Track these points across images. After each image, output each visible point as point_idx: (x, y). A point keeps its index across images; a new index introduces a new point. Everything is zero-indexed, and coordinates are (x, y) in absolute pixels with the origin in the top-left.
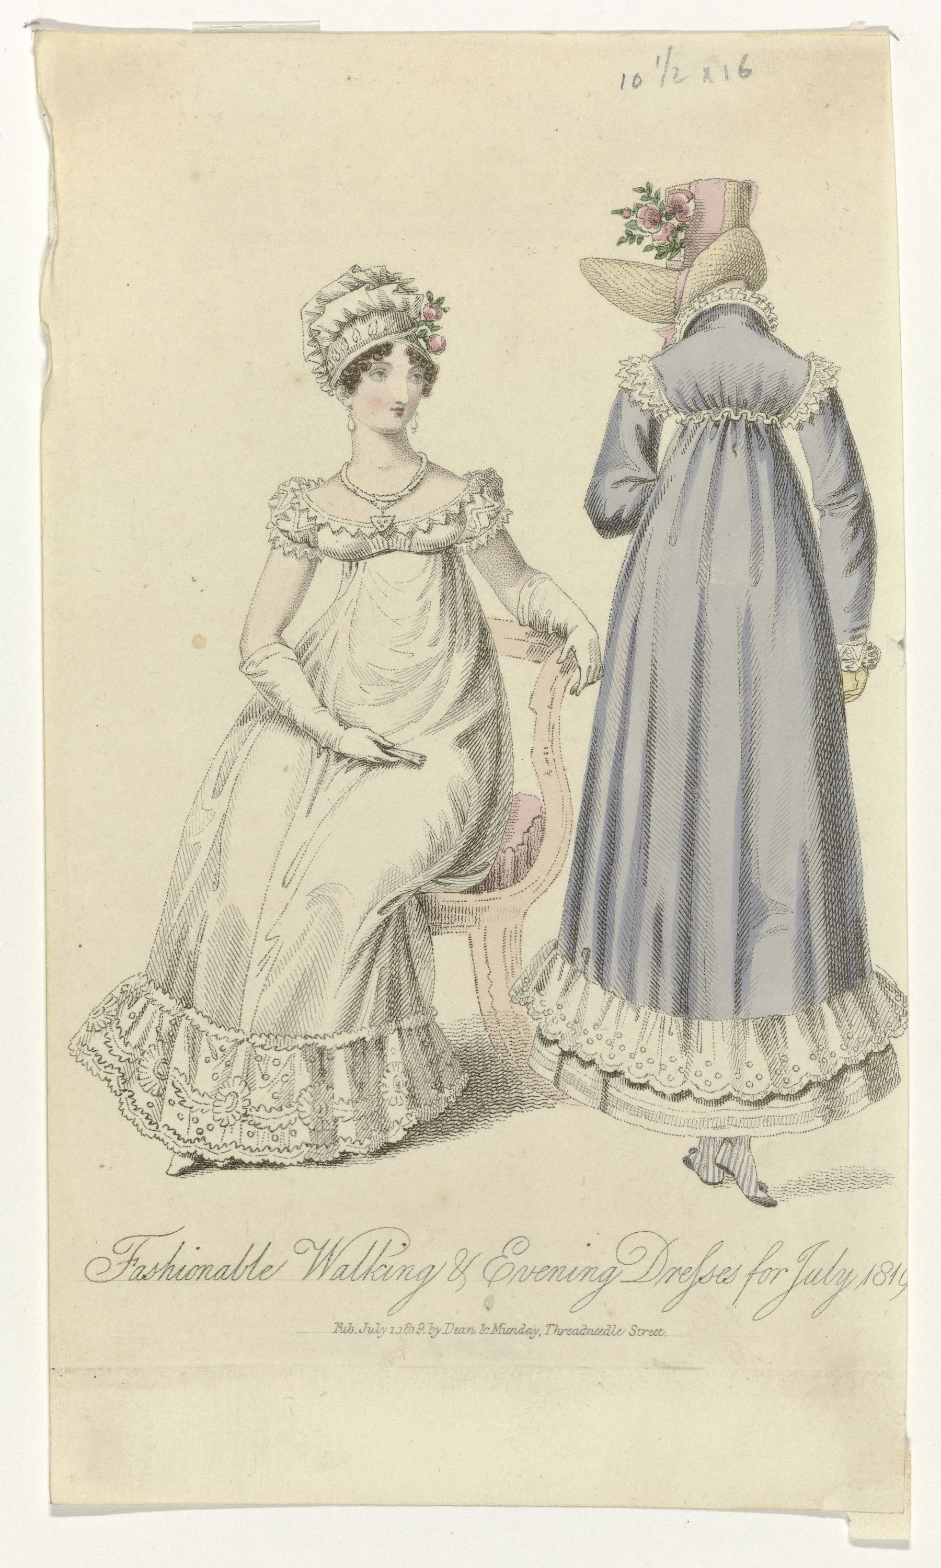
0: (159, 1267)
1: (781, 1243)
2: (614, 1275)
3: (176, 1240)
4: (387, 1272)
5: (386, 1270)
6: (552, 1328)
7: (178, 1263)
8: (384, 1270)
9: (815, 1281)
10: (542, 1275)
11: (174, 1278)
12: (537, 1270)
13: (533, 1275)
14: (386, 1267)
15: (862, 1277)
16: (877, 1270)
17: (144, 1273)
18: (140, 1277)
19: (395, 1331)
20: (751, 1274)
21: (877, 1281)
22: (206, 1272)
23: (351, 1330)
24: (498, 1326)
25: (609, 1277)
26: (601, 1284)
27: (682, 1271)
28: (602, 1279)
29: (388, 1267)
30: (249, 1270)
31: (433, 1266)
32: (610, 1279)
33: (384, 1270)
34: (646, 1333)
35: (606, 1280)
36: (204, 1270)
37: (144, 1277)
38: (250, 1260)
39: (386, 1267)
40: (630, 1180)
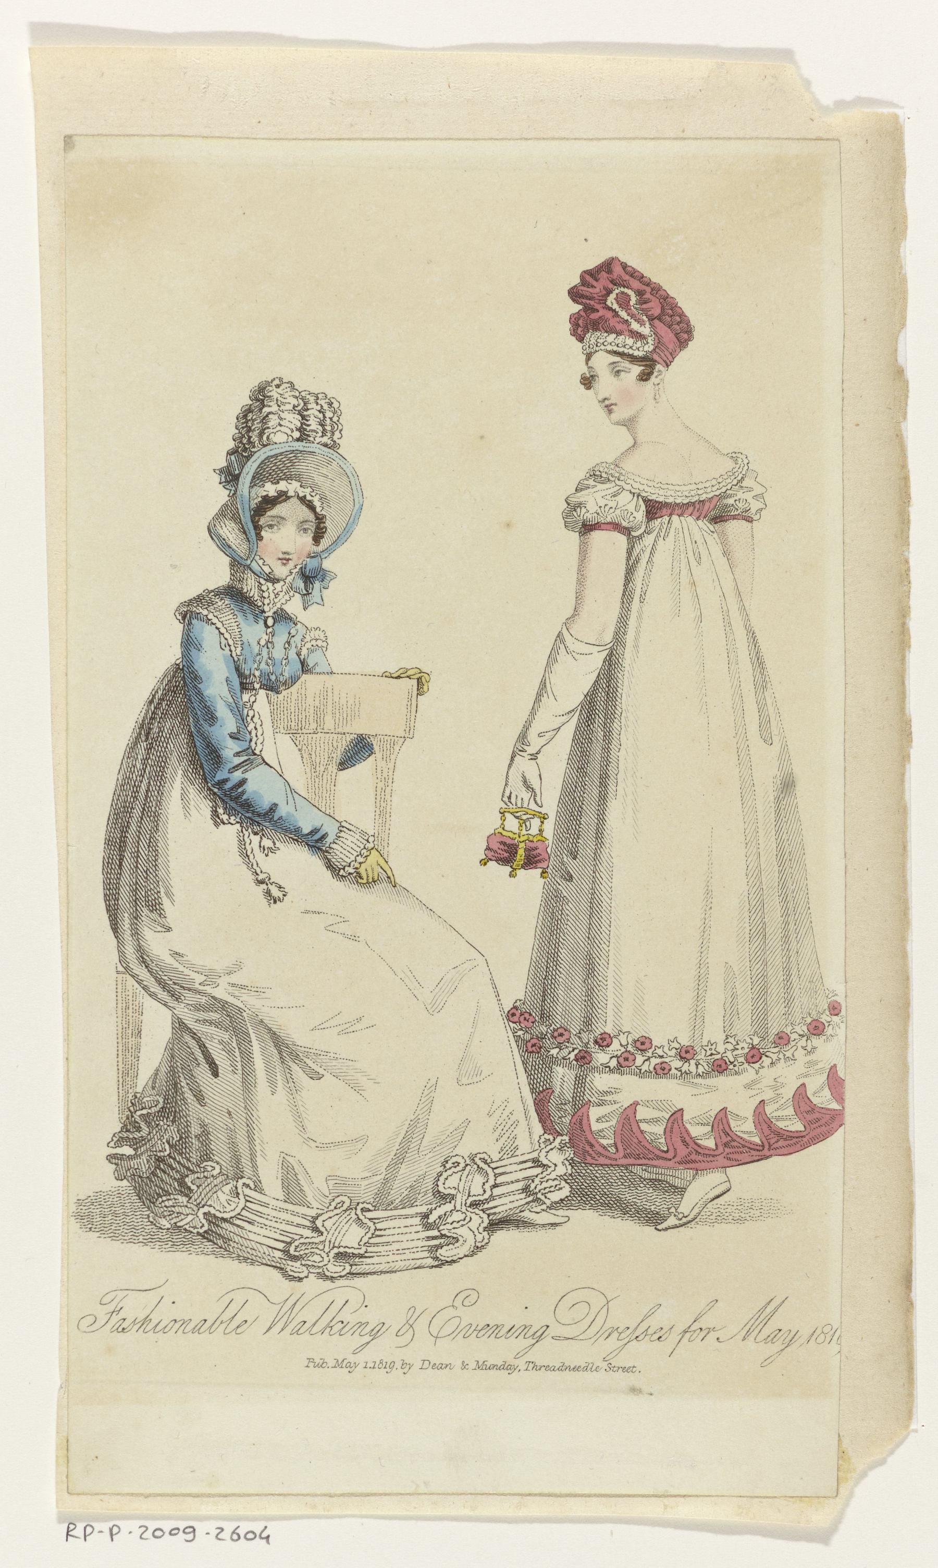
0: (137, 1321)
1: (567, 1219)
2: (383, 1329)
3: (153, 1297)
4: (343, 1328)
5: (343, 1325)
6: (531, 1365)
7: (155, 1319)
8: (340, 1326)
9: (314, 1330)
10: (483, 1332)
11: (503, 1337)
12: (479, 1328)
13: (476, 1333)
14: (342, 1322)
15: (806, 1337)
16: (818, 1332)
17: (124, 1325)
18: (120, 1329)
19: (368, 1366)
20: (685, 1332)
21: (819, 1340)
22: (184, 1326)
23: (321, 1365)
24: (480, 1363)
25: (542, 1335)
26: (535, 1341)
27: (620, 1330)
28: (535, 1337)
29: (345, 1323)
30: (224, 1325)
31: (384, 1324)
32: (543, 1337)
33: (340, 1326)
34: (543, 1369)
35: (539, 1337)
36: (181, 1324)
37: (123, 1329)
38: (225, 1317)
39: (342, 1322)
40: (876, 1237)
